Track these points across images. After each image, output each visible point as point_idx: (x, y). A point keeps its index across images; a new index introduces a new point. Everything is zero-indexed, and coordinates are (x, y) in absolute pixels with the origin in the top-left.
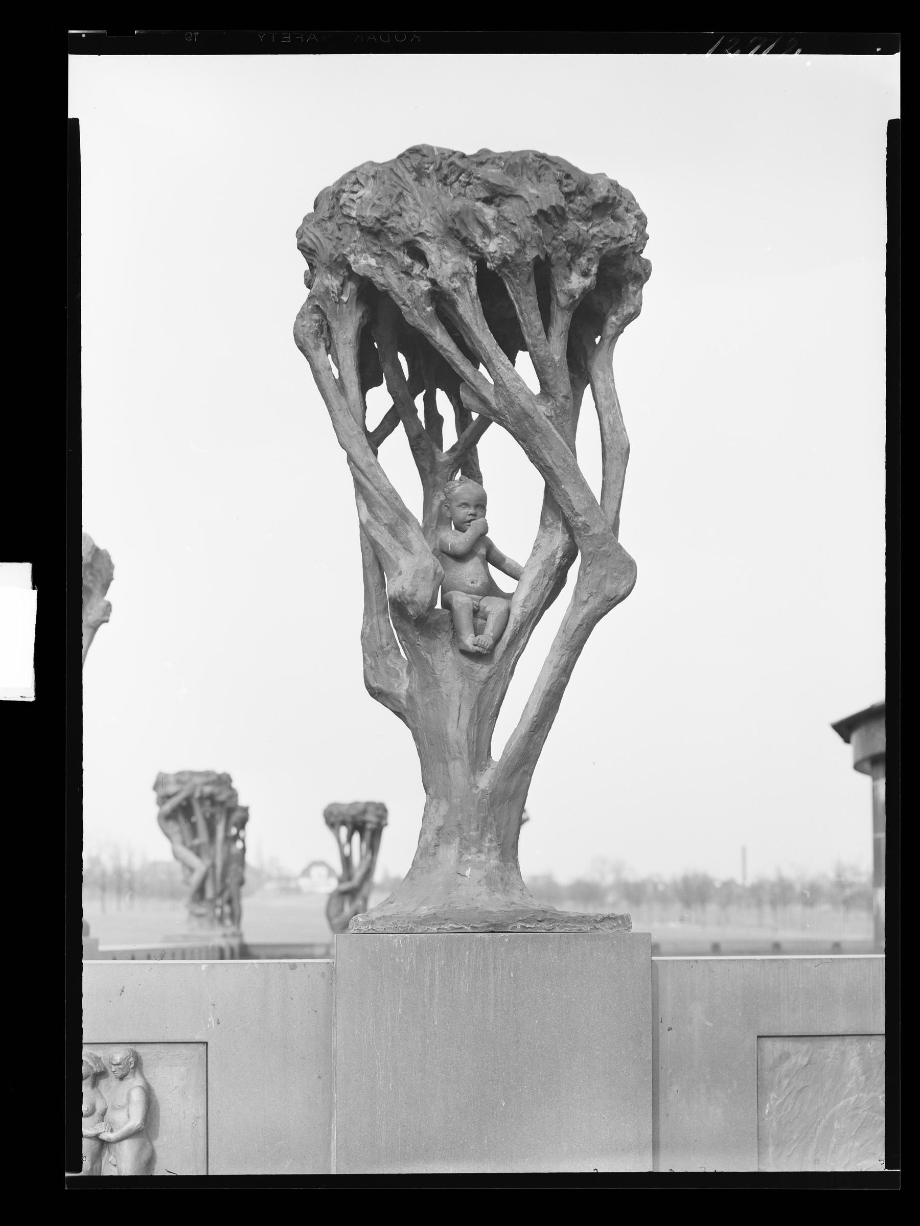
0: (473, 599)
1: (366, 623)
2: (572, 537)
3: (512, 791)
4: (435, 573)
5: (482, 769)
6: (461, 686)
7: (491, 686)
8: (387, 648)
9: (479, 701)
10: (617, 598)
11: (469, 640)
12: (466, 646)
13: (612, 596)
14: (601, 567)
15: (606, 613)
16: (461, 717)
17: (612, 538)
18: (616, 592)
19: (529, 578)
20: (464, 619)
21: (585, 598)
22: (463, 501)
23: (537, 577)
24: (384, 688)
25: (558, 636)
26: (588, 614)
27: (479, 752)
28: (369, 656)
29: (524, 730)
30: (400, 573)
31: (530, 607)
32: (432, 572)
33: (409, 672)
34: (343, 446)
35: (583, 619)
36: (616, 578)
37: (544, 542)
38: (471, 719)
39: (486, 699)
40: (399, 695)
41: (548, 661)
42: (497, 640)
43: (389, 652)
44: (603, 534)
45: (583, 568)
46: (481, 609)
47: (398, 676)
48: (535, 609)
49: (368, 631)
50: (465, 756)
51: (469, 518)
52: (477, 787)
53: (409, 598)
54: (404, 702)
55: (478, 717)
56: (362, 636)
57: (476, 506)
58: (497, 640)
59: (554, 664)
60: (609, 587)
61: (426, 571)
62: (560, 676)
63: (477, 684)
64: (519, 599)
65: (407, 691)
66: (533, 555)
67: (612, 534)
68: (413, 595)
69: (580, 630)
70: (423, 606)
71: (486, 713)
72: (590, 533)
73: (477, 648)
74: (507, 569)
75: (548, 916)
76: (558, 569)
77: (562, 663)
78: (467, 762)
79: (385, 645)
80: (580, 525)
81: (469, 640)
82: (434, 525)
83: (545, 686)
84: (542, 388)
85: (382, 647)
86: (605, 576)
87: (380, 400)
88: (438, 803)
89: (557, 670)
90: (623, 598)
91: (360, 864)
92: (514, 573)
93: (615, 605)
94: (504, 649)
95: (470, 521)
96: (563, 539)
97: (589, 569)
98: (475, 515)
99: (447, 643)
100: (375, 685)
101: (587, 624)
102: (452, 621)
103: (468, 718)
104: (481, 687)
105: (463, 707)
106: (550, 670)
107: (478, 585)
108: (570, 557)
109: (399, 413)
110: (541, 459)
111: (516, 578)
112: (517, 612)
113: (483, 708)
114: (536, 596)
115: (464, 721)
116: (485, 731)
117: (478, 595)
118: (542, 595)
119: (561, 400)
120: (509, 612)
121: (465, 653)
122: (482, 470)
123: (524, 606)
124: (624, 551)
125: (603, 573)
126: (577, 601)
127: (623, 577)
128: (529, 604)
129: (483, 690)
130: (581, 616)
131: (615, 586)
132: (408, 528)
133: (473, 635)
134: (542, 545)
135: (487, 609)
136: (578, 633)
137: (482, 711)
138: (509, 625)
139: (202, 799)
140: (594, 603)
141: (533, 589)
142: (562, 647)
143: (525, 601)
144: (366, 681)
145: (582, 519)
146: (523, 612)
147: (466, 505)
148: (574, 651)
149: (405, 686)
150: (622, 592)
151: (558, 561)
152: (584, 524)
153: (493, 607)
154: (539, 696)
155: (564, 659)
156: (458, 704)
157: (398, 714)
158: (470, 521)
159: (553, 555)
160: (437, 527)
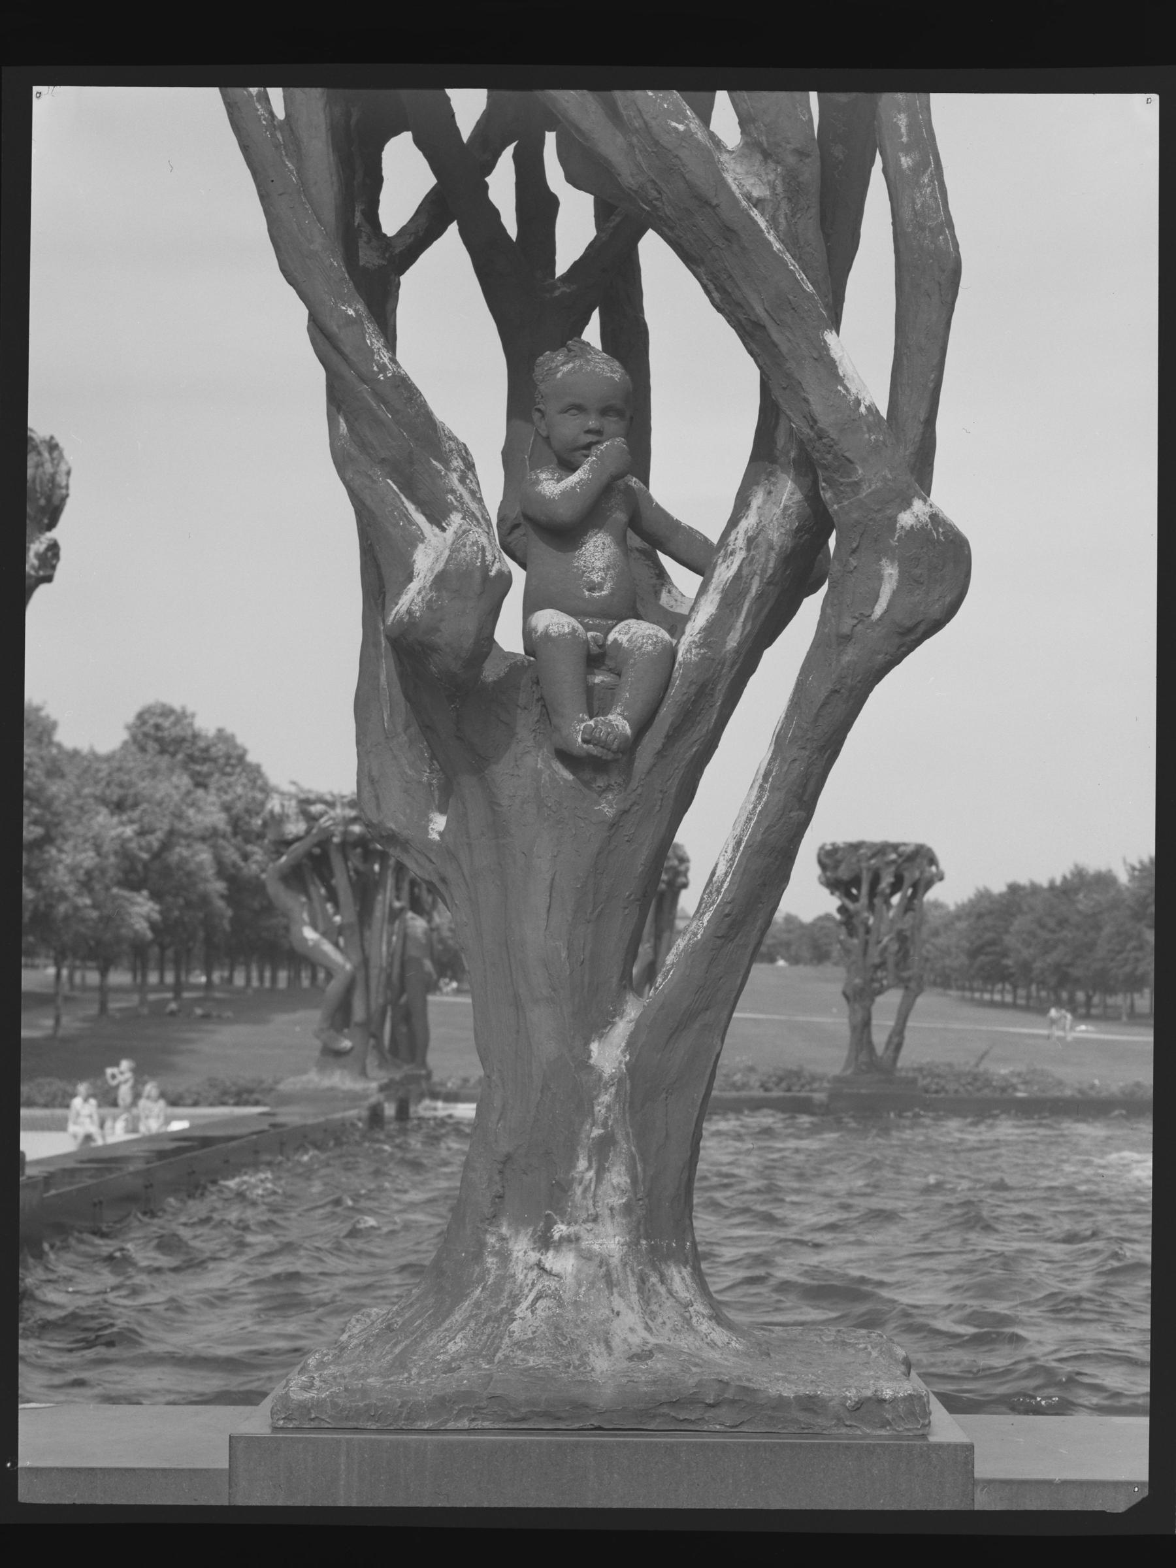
11: (579, 729)
22: (569, 400)
34: (291, 281)
51: (590, 438)
75: (729, 1395)
84: (744, 132)
87: (405, 177)
91: (699, 912)
93: (919, 642)
94: (659, 746)
95: (588, 446)
97: (854, 562)
98: (599, 432)
109: (455, 198)
110: (739, 305)
119: (791, 160)
121: (566, 757)
122: (649, 317)
139: (346, 846)
147: (580, 408)
148: (822, 749)
150: (936, 610)
158: (588, 446)
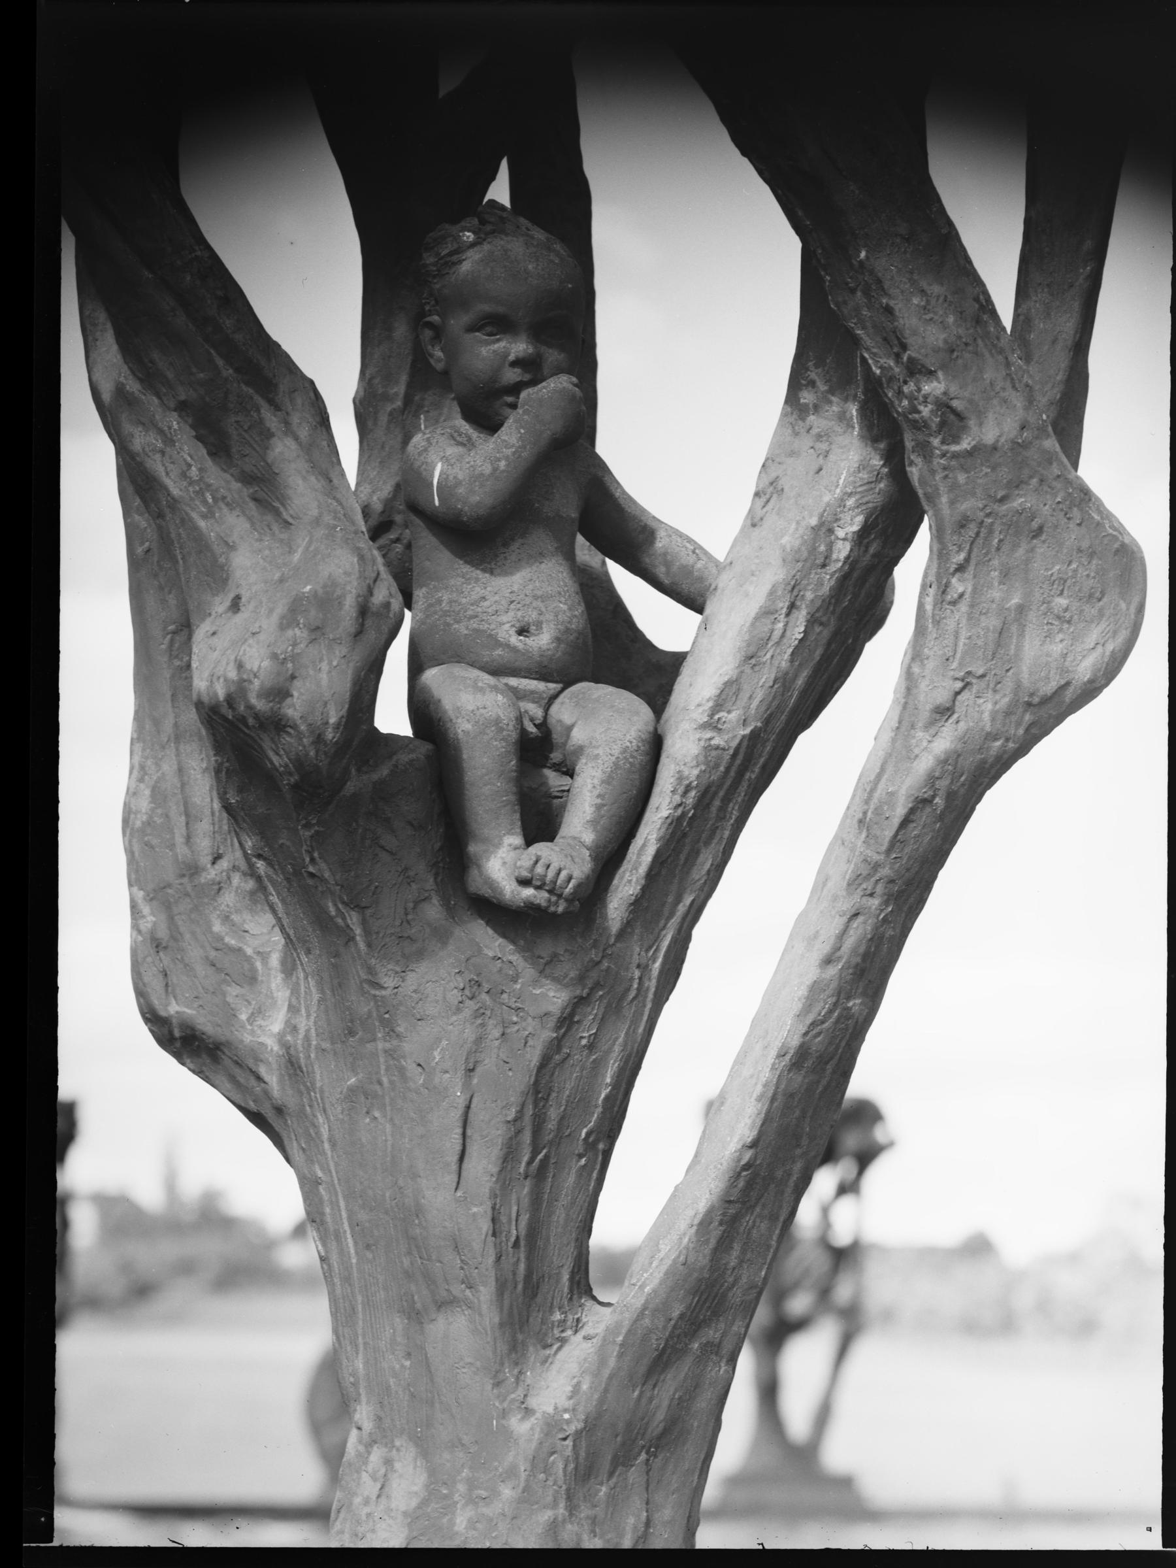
0: (518, 695)
1: (139, 772)
2: (895, 458)
3: (661, 1415)
4: (364, 611)
5: (548, 1340)
6: (470, 1034)
7: (585, 1033)
8: (212, 873)
9: (539, 1090)
10: (1069, 695)
12: (490, 883)
13: (1049, 688)
14: (1006, 574)
15: (1022, 750)
16: (473, 1150)
17: (1049, 459)
18: (1063, 671)
19: (738, 609)
20: (486, 771)
21: (941, 696)
22: (487, 308)
23: (767, 612)
24: (206, 1024)
25: (839, 840)
26: (950, 761)
27: (545, 1271)
28: (150, 899)
29: (706, 1194)
30: (236, 605)
31: (737, 726)
32: (349, 605)
33: (288, 969)
35: (931, 779)
36: (1064, 619)
37: (795, 472)
38: (509, 1155)
39: (567, 1083)
40: (257, 1053)
41: (801, 930)
42: (610, 858)
43: (218, 888)
44: (1018, 447)
45: (938, 583)
46: (557, 737)
47: (251, 979)
48: (754, 736)
49: (144, 804)
50: (486, 1293)
51: (512, 375)
52: (528, 1412)
53: (260, 705)
54: (273, 1080)
55: (535, 1153)
56: (126, 822)
57: (540, 332)
58: (610, 858)
59: (823, 948)
60: (1040, 655)
61: (326, 600)
62: (843, 993)
63: (531, 1025)
64: (694, 692)
65: (280, 1038)
66: (754, 522)
67: (1051, 443)
68: (280, 693)
69: (924, 816)
70: (319, 739)
71: (566, 1130)
72: (965, 444)
73: (528, 892)
74: (661, 572)
76: (844, 579)
77: (849, 943)
78: (490, 1316)
79: (206, 860)
80: (926, 411)
81: (503, 863)
82: (400, 389)
83: (786, 1031)
85: (192, 870)
86: (1021, 609)
88: (388, 1462)
89: (833, 971)
90: (1090, 691)
92: (685, 587)
96: (862, 467)
97: (958, 585)
99: (420, 868)
100: (173, 1008)
101: (950, 796)
102: (167, 985)
103: (496, 1152)
104: (548, 1034)
105: (479, 1116)
106: (808, 971)
107: (543, 640)
108: (889, 529)
111: (695, 603)
112: (685, 750)
113: (553, 1114)
114: (758, 690)
115: (483, 1165)
116: (564, 1200)
117: (544, 677)
118: (783, 681)
120: (656, 745)
123: (712, 725)
124: (1100, 507)
125: (1015, 600)
126: (911, 715)
127: (1091, 611)
128: (731, 717)
129: (556, 1045)
130: (924, 764)
131: (1057, 648)
132: (272, 421)
133: (517, 840)
134: (784, 482)
135: (578, 736)
136: (914, 830)
137: (551, 1125)
138: (654, 801)
140: (982, 710)
141: (751, 658)
142: (854, 882)
143: (719, 704)
144: (141, 993)
145: (933, 387)
146: (708, 748)
147: (499, 324)
149: (276, 1023)
150: (1084, 669)
151: (842, 550)
152: (943, 406)
153: (598, 725)
154: (763, 1071)
155: (861, 929)
156: (461, 1103)
157: (257, 1119)
159: (825, 528)
160: (408, 400)
